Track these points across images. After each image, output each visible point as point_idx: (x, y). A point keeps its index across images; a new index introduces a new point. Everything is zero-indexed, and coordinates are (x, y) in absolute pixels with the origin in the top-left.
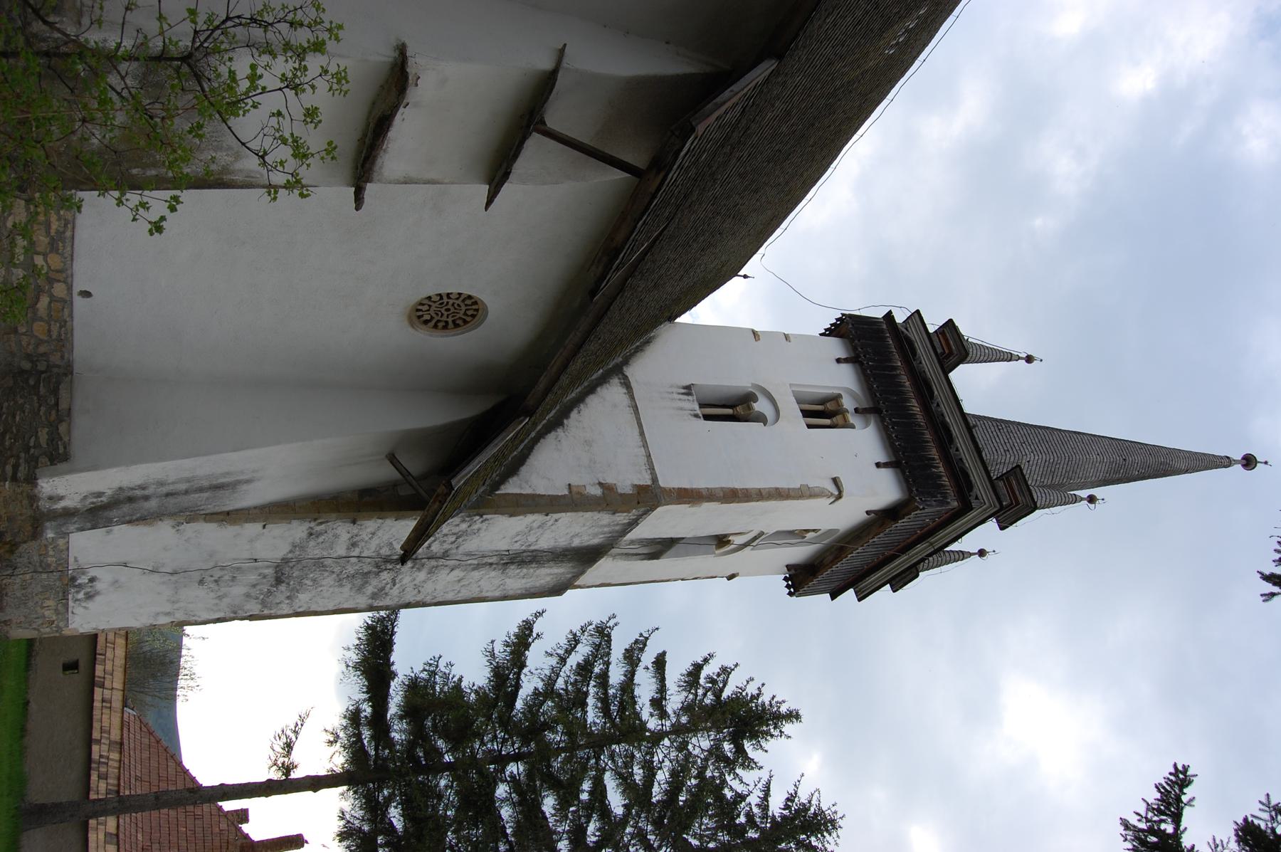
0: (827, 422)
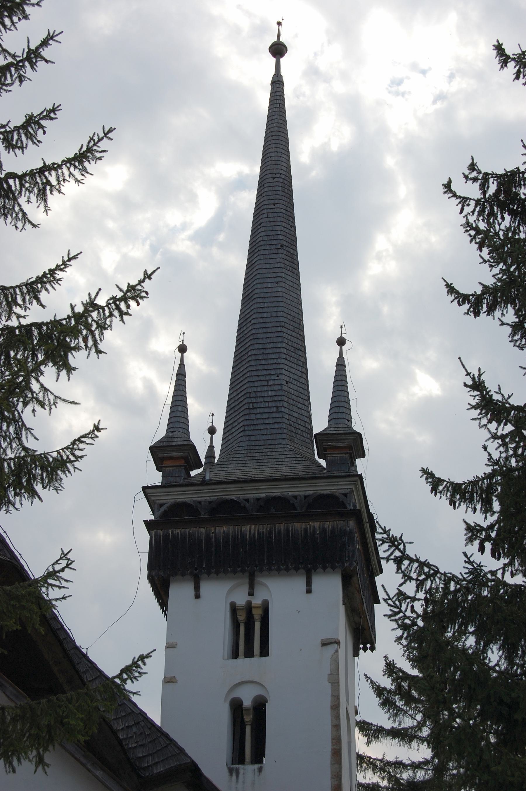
0: (257, 626)
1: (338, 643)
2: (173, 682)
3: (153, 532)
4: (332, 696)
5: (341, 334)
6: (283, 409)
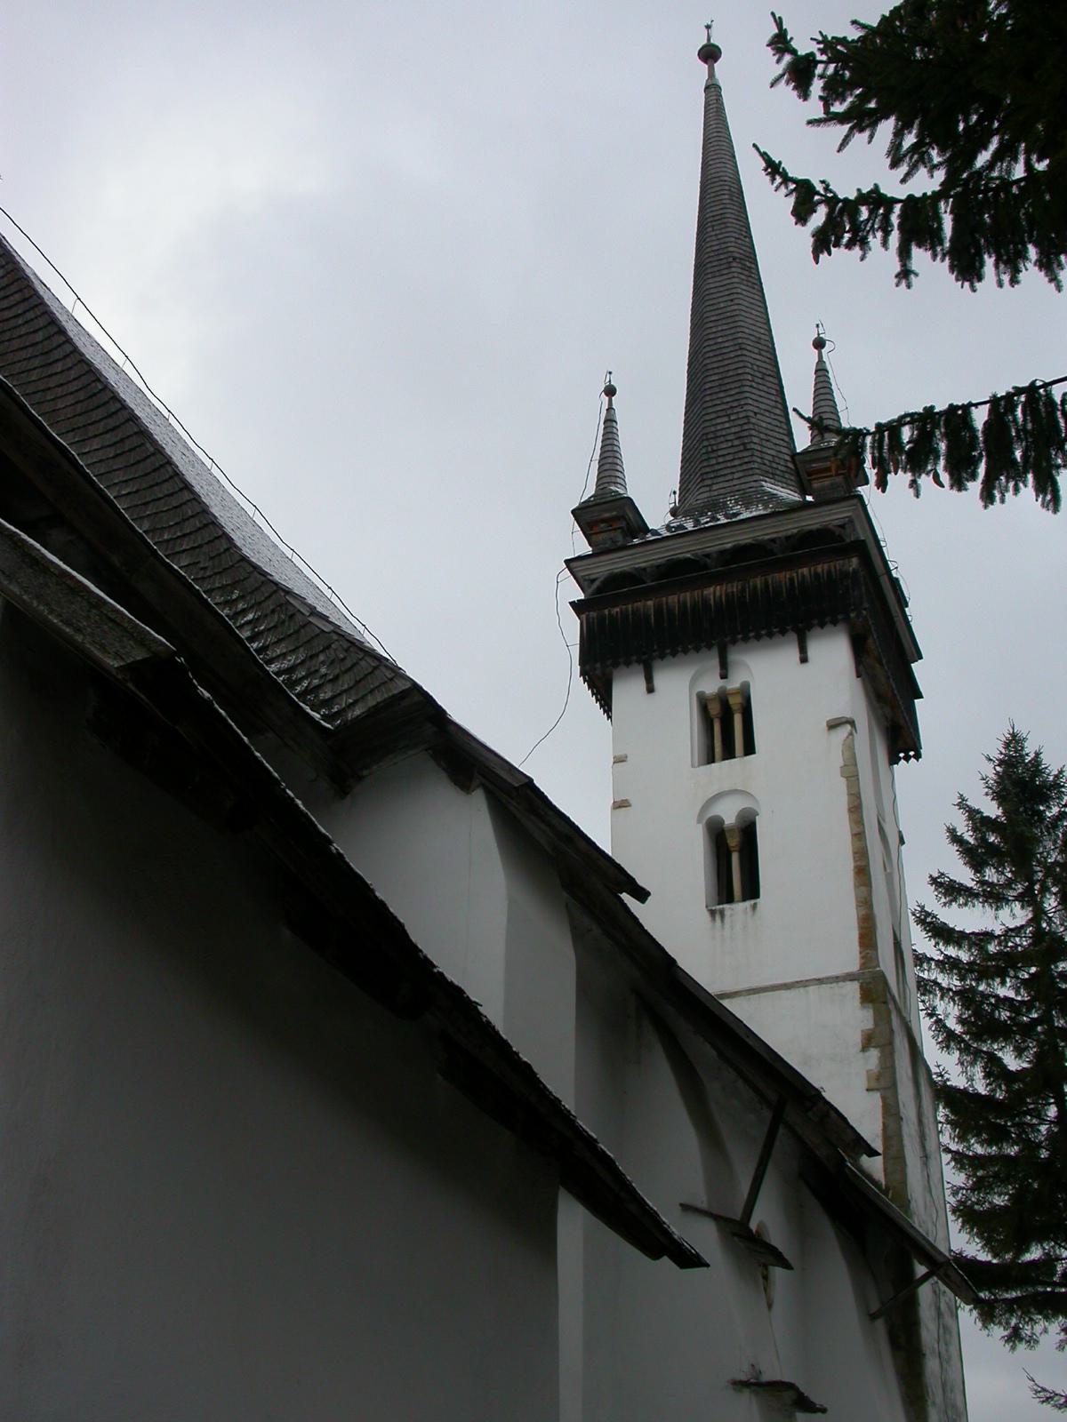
1: (852, 723)
3: (584, 616)
4: (850, 794)
5: (819, 334)
6: (753, 446)
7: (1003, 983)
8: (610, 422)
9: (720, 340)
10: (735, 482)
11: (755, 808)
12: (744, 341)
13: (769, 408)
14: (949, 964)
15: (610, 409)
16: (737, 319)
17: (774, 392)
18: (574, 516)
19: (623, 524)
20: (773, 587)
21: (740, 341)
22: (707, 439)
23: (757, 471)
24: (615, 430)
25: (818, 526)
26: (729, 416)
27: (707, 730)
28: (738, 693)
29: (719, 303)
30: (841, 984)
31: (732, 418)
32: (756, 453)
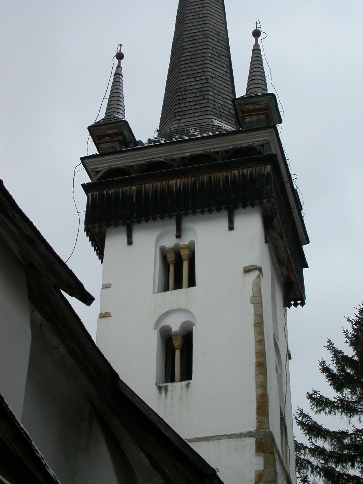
0: (186, 266)
1: (260, 270)
2: (107, 317)
3: (90, 194)
5: (257, 28)
6: (209, 97)
7: (353, 466)
8: (118, 75)
9: (193, 31)
10: (196, 118)
11: (193, 321)
12: (209, 32)
13: (222, 76)
14: (318, 451)
15: (119, 67)
16: (205, 19)
17: (226, 66)
18: (90, 131)
19: (121, 138)
20: (214, 181)
21: (206, 32)
22: (180, 91)
23: (211, 113)
24: (121, 81)
25: (246, 145)
26: (195, 78)
27: (127, 152)
28: (187, 248)
29: (195, 8)
30: (243, 439)
31: (197, 79)
32: (210, 102)
